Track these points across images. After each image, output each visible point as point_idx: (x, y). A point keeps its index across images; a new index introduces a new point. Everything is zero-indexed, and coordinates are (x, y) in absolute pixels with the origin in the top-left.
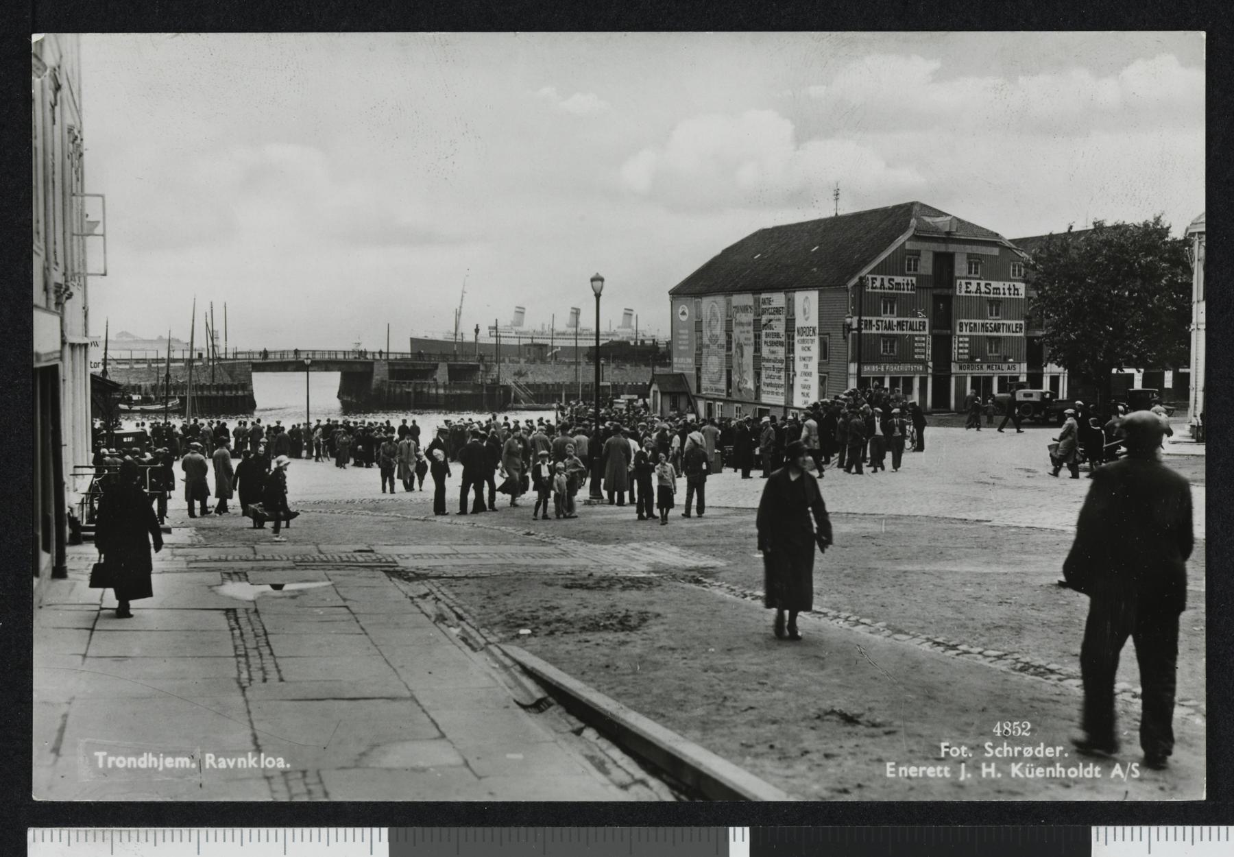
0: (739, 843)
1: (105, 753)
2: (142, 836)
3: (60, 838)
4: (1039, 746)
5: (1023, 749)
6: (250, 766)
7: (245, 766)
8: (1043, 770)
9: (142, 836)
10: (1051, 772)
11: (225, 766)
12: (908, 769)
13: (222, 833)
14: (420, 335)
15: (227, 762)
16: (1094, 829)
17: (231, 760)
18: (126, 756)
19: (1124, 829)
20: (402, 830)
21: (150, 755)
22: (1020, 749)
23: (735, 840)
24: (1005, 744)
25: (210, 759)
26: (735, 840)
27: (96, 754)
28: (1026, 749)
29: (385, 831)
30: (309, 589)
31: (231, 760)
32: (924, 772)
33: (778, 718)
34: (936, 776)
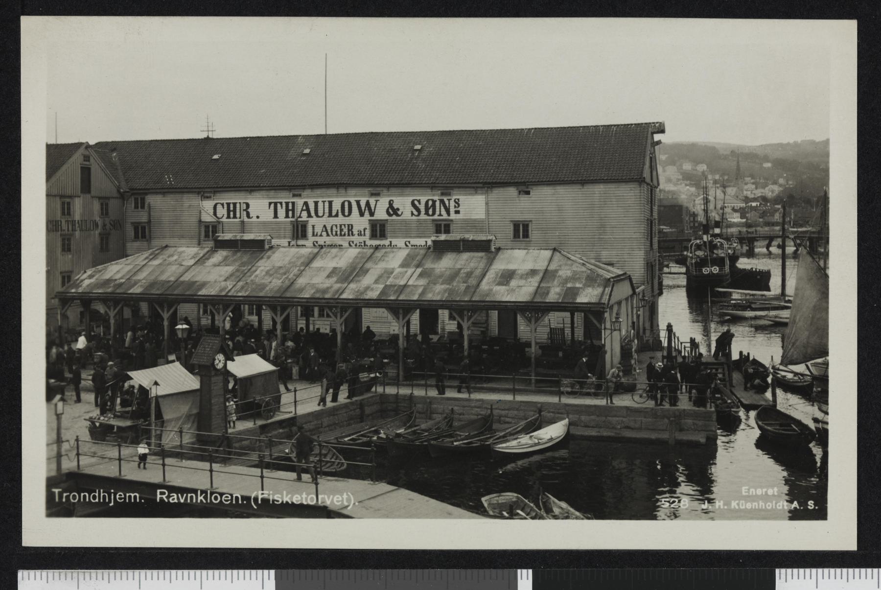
0: (525, 581)
2: (100, 576)
3: (860, 577)
9: (100, 576)
11: (176, 501)
13: (816, 572)
16: (777, 571)
19: (811, 570)
20: (284, 571)
23: (521, 579)
26: (521, 579)
29: (272, 572)
31: (329, 498)
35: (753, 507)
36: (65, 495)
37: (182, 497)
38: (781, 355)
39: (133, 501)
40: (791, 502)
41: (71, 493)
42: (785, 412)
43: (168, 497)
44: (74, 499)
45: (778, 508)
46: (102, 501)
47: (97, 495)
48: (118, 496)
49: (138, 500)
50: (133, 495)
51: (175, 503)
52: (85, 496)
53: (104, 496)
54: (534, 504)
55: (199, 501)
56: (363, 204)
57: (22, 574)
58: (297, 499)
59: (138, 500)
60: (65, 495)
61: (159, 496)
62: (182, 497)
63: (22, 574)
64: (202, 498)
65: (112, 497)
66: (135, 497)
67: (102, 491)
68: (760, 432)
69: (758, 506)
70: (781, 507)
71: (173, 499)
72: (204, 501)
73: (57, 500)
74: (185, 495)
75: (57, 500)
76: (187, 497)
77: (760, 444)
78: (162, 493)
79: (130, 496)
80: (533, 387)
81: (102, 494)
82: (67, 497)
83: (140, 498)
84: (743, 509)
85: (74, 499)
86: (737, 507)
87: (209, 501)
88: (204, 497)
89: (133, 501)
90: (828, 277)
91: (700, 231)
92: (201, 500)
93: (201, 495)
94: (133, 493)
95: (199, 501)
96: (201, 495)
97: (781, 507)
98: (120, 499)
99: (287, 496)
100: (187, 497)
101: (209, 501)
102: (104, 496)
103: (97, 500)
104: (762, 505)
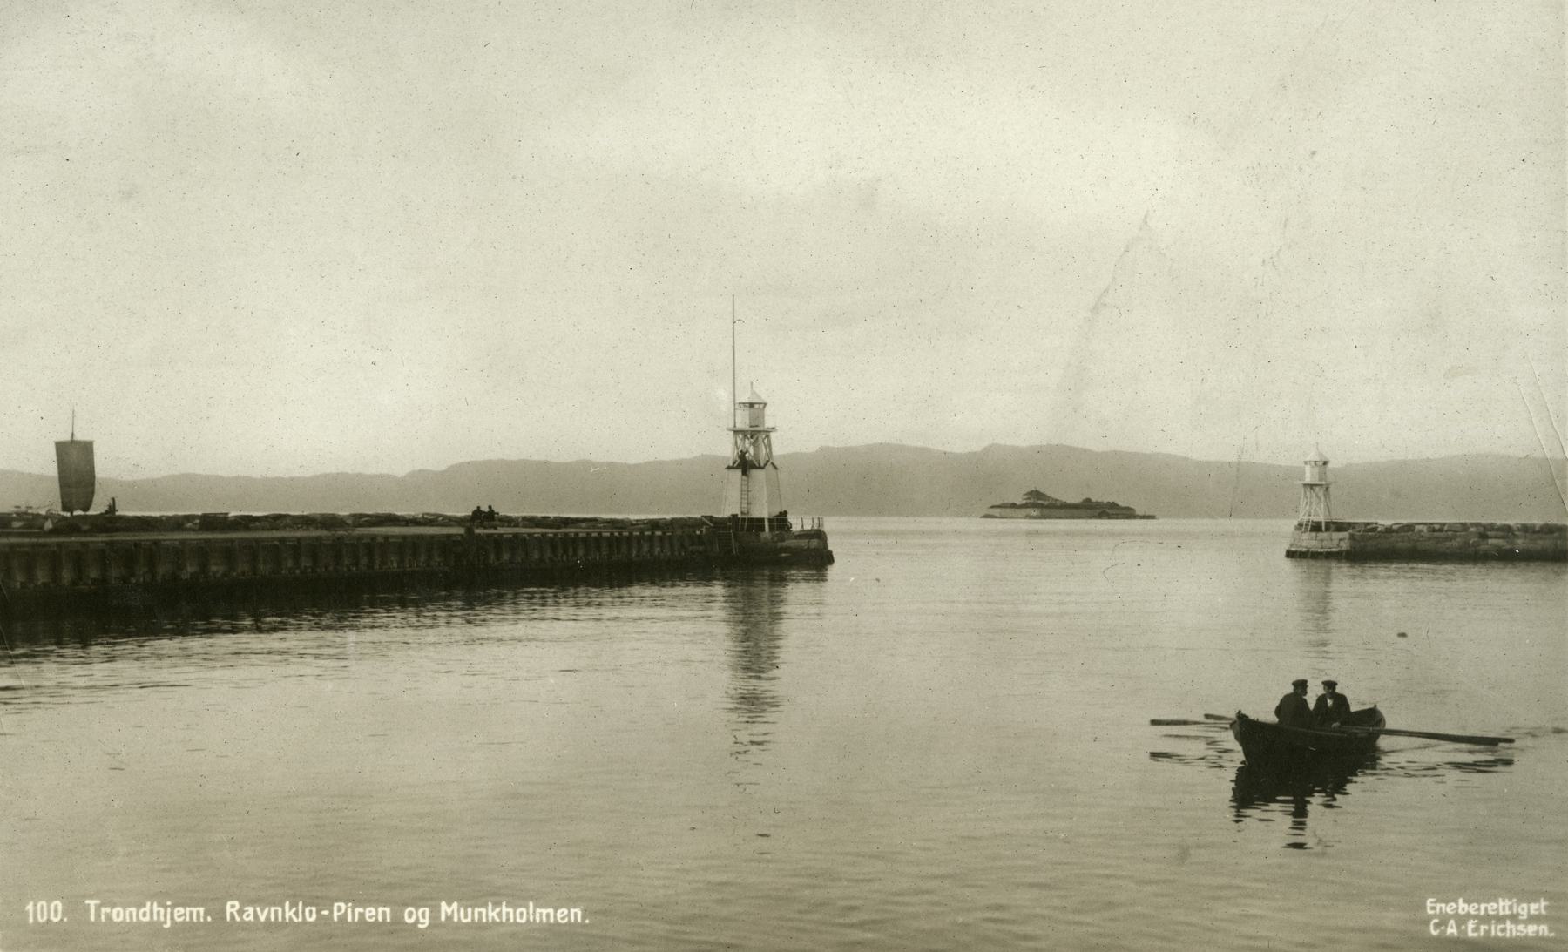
1: (98, 902)
4: (338, 917)
5: (365, 910)
6: (490, 920)
7: (552, 920)
8: (566, 911)
10: (480, 913)
11: (251, 918)
12: (556, 912)
14: (95, 446)
15: (255, 912)
17: (262, 911)
18: (125, 906)
21: (155, 904)
22: (361, 910)
24: (504, 904)
25: (232, 907)
27: (87, 902)
28: (368, 909)
30: (88, 542)
31: (262, 911)
32: (362, 915)
33: (1552, 735)
34: (1498, 914)
35: (538, 920)
36: (103, 910)
42: (1464, 734)
43: (241, 912)
44: (410, 917)
45: (141, 918)
47: (147, 909)
48: (176, 915)
50: (195, 910)
51: (250, 921)
54: (63, 909)
55: (490, 920)
56: (560, 552)
58: (371, 914)
64: (494, 914)
66: (198, 913)
68: (1353, 708)
69: (152, 905)
70: (147, 919)
71: (248, 916)
73: (92, 918)
75: (92, 918)
76: (269, 913)
78: (233, 906)
79: (541, 914)
80: (143, 543)
83: (206, 914)
84: (467, 924)
85: (410, 917)
86: (498, 920)
92: (493, 918)
93: (290, 909)
97: (251, 918)
101: (504, 920)
102: (158, 913)
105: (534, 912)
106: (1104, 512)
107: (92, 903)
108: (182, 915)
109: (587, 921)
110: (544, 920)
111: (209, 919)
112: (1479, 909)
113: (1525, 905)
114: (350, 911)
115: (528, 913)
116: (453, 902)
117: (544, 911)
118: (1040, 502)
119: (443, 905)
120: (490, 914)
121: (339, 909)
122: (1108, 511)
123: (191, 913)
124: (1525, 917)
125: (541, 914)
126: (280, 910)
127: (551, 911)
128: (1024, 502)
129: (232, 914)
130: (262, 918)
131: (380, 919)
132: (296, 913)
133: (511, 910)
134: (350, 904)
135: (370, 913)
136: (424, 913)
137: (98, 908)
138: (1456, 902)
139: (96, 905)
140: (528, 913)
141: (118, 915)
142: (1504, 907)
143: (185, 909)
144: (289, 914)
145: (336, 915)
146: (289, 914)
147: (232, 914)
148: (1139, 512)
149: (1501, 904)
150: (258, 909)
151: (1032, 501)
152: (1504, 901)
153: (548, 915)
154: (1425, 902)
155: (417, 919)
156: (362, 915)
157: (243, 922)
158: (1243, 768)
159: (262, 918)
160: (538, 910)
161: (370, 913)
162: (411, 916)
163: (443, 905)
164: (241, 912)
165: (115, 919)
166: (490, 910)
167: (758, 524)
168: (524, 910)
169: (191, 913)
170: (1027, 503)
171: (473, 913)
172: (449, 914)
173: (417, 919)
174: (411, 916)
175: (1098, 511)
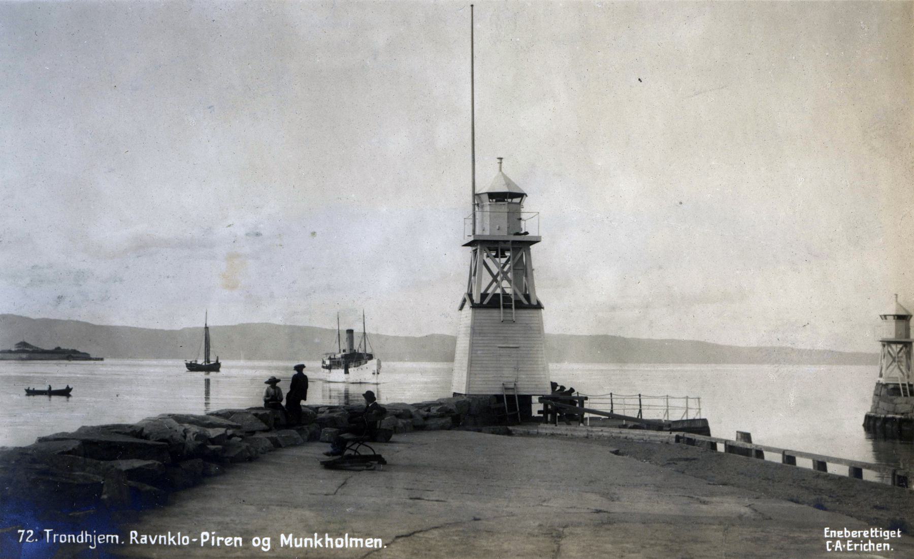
6: (316, 546)
21: (86, 532)
22: (222, 539)
27: (45, 530)
37: (153, 539)
38: (62, 347)
39: (112, 542)
40: (543, 399)
41: (60, 535)
46: (86, 541)
47: (82, 535)
48: (99, 539)
49: (117, 542)
52: (71, 538)
53: (88, 537)
55: (316, 546)
57: (533, 415)
59: (117, 542)
60: (55, 535)
61: (132, 538)
62: (153, 539)
63: (533, 415)
64: (172, 539)
65: (95, 539)
66: (115, 539)
67: (86, 532)
72: (321, 546)
74: (156, 536)
77: (305, 399)
79: (354, 542)
81: (87, 535)
82: (58, 538)
86: (321, 546)
87: (179, 543)
88: (321, 542)
89: (112, 542)
90: (864, 425)
91: (558, 416)
92: (318, 545)
94: (113, 535)
95: (169, 543)
96: (171, 537)
97: (146, 542)
98: (101, 541)
99: (171, 537)
100: (158, 538)
101: (179, 543)
102: (88, 537)
103: (82, 541)
104: (329, 542)
105: (349, 541)
106: (70, 355)
107: (48, 531)
108: (103, 540)
109: (892, 549)
110: (356, 546)
111: (892, 549)
112: (857, 534)
113: (888, 532)
114: (213, 538)
115: (344, 542)
116: (280, 535)
117: (356, 540)
118: (26, 349)
119: (283, 536)
120: (170, 540)
121: (205, 537)
122: (72, 355)
123: (110, 538)
124: (848, 541)
125: (354, 542)
126: (165, 537)
127: (361, 540)
128: (16, 349)
129: (133, 540)
130: (153, 542)
131: (376, 547)
132: (176, 540)
133: (331, 540)
134: (213, 533)
135: (228, 541)
136: (266, 542)
137: (51, 534)
138: (843, 530)
139: (50, 532)
140: (344, 542)
141: (63, 539)
142: (874, 534)
143: (374, 539)
144: (171, 539)
145: (203, 541)
146: (171, 539)
147: (133, 540)
148: (92, 356)
149: (872, 531)
150: (150, 537)
151: (21, 348)
152: (874, 530)
153: (359, 542)
154: (824, 529)
155: (261, 545)
156: (222, 542)
157: (140, 544)
158: (389, 439)
159: (153, 542)
160: (351, 540)
161: (228, 541)
162: (256, 542)
163: (283, 536)
164: (139, 539)
165: (61, 541)
166: (316, 538)
167: (743, 498)
168: (342, 540)
169: (110, 538)
170: (18, 350)
171: (84, 540)
172: (286, 544)
173: (261, 545)
174: (256, 542)
175: (67, 355)
